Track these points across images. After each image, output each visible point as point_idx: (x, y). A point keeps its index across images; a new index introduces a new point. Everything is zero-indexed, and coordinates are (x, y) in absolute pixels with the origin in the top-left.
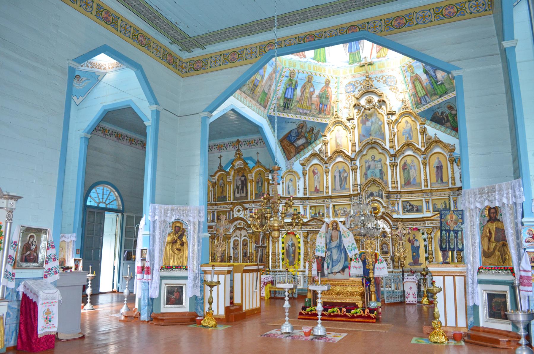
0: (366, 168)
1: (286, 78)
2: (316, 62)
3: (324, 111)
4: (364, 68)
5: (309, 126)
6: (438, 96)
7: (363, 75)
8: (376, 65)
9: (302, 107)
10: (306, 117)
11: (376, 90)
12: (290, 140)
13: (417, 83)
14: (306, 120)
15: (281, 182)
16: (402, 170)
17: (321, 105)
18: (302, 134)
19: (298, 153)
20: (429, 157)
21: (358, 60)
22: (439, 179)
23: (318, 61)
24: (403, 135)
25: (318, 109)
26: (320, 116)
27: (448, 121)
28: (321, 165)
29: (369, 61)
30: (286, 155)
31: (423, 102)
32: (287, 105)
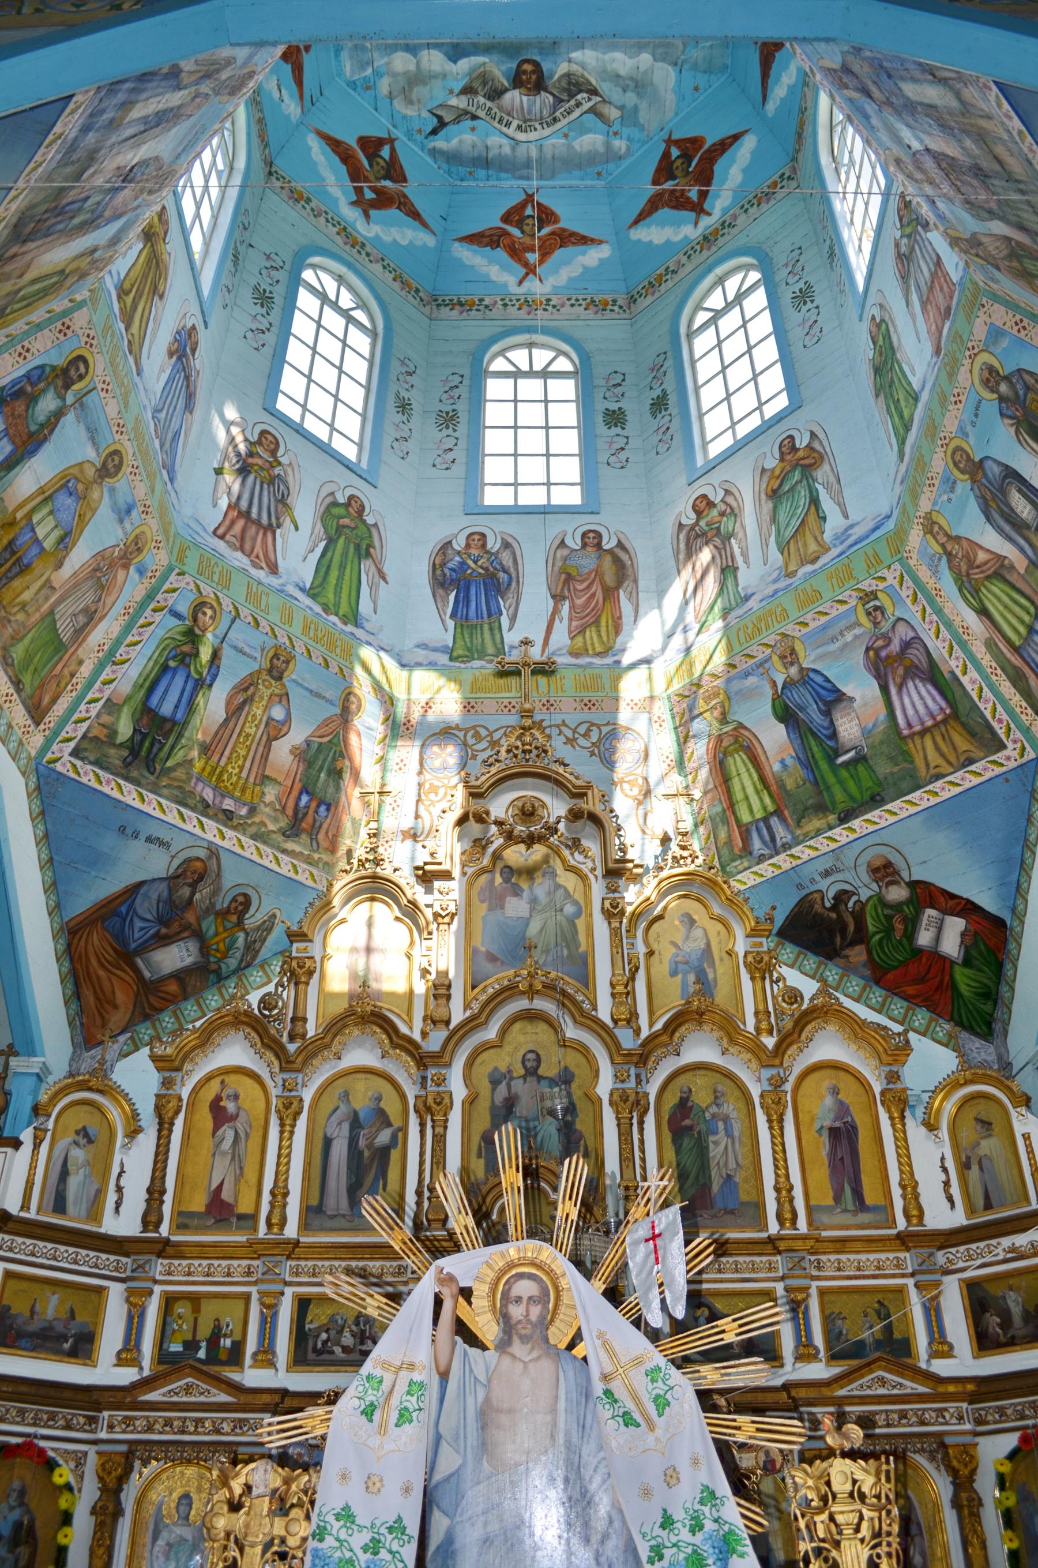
0: (493, 1108)
1: (175, 622)
2: (318, 609)
3: (313, 832)
4: (513, 681)
5: (231, 879)
6: (832, 818)
7: (509, 707)
8: (567, 679)
9: (216, 778)
10: (229, 833)
11: (561, 770)
12: (120, 938)
13: (738, 764)
14: (226, 844)
15: (27, 1136)
16: (667, 1137)
17: (305, 799)
18: (190, 917)
19: (146, 1017)
20: (792, 1079)
21: (491, 650)
22: (848, 1190)
23: (326, 609)
24: (674, 973)
25: (290, 811)
26: (290, 846)
27: (861, 937)
28: (265, 1075)
29: (536, 653)
30: (82, 1011)
31: (757, 844)
32: (147, 744)
